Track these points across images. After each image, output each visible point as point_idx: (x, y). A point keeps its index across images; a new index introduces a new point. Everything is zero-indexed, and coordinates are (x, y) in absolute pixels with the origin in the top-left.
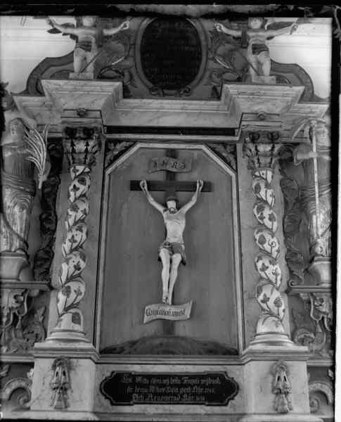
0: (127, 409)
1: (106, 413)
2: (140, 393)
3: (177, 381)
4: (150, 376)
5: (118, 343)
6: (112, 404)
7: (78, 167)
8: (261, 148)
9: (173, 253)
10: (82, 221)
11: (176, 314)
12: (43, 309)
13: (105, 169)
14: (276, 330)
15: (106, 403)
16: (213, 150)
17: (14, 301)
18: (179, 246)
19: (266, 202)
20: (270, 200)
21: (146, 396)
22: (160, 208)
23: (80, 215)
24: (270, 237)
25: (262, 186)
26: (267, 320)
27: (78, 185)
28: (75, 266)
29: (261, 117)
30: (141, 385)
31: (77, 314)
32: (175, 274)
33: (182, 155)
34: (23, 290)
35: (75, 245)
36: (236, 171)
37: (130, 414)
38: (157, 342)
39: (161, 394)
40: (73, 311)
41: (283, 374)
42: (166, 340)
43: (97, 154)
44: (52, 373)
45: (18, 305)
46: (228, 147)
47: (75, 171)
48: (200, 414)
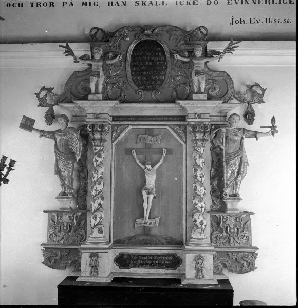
0: (127, 271)
1: (117, 273)
2: (133, 263)
3: (152, 258)
4: (138, 255)
5: (123, 237)
6: (120, 268)
7: (97, 148)
8: (198, 136)
9: (149, 194)
10: (101, 177)
11: (151, 224)
12: (84, 221)
13: (112, 142)
14: (199, 237)
15: (117, 267)
16: (173, 129)
17: (69, 219)
18: (152, 189)
19: (199, 166)
20: (201, 165)
21: (136, 264)
22: (143, 167)
23: (99, 175)
24: (199, 187)
25: (198, 157)
26: (196, 231)
27: (97, 159)
28: (98, 205)
29: (199, 116)
30: (134, 260)
31: (101, 228)
32: (150, 204)
33: (156, 132)
34: (117, 4)
35: (98, 192)
36: (185, 142)
37: (129, 273)
38: (142, 238)
39: (143, 264)
40: (98, 227)
41: (200, 261)
42: (146, 237)
43: (119, 92)
44: (89, 259)
45: (71, 221)
46: (182, 127)
47: (96, 150)
48: (163, 274)
